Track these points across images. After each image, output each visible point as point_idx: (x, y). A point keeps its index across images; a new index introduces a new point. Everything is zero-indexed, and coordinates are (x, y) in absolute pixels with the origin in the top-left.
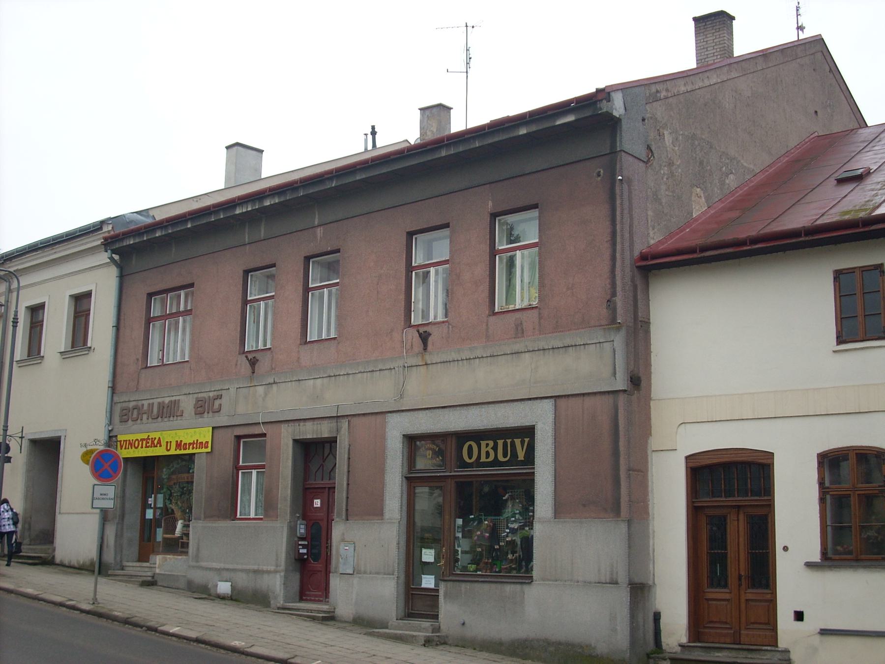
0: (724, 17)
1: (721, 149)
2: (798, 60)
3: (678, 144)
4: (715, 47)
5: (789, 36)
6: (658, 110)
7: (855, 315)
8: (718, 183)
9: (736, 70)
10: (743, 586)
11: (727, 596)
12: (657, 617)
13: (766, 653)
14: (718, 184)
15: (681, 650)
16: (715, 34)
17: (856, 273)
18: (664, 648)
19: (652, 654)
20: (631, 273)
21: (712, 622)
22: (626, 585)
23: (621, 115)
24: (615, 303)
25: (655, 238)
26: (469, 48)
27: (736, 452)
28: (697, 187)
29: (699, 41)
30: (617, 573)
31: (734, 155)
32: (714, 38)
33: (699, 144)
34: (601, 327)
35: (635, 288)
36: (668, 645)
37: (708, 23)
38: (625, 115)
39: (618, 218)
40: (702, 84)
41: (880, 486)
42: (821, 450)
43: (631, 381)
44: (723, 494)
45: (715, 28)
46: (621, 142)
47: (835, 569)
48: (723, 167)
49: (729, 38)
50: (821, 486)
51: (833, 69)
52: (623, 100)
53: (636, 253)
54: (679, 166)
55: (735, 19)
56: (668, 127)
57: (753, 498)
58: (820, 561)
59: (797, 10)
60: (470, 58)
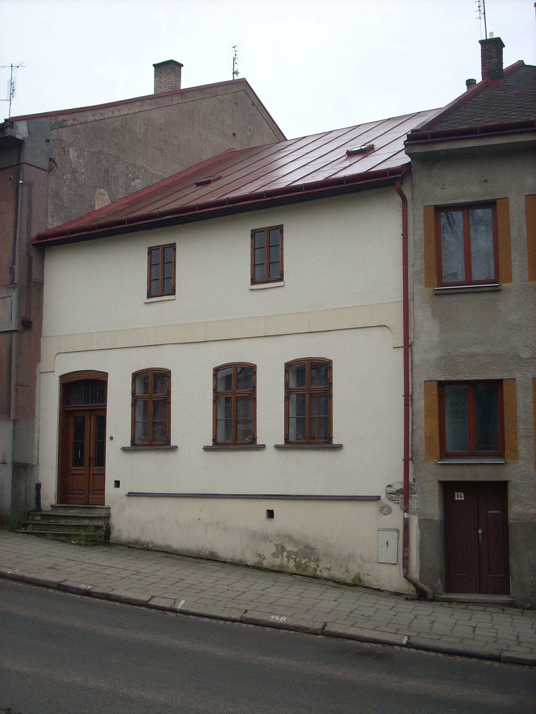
0: (173, 64)
1: (128, 161)
2: (219, 97)
3: (83, 157)
4: (166, 86)
5: (229, 77)
6: (65, 134)
7: (170, 277)
8: (123, 185)
9: (149, 104)
10: (92, 465)
11: (83, 472)
12: (38, 487)
13: (98, 509)
14: (124, 186)
15: (52, 510)
16: (167, 77)
17: (160, 249)
18: (42, 508)
19: (31, 512)
20: (27, 248)
21: (74, 490)
22: (10, 465)
23: (24, 138)
24: (14, 269)
25: (54, 224)
26: (14, 82)
27: (88, 373)
28: (101, 188)
29: (156, 82)
30: (6, 456)
31: (142, 165)
32: (166, 79)
33: (105, 158)
34: (5, 287)
35: (30, 260)
36: (44, 506)
37: (163, 69)
38: (28, 137)
39: (19, 210)
40: (112, 115)
41: (165, 395)
42: (134, 371)
43: (22, 324)
44: (98, 401)
45: (167, 72)
46: (23, 156)
47: (138, 452)
48: (129, 174)
49: (177, 79)
50: (286, 399)
51: (256, 103)
52: (27, 127)
53: (34, 234)
54: (83, 173)
55: (183, 66)
56: (73, 146)
57: (99, 404)
58: (130, 446)
59: (234, 60)
60: (14, 90)
